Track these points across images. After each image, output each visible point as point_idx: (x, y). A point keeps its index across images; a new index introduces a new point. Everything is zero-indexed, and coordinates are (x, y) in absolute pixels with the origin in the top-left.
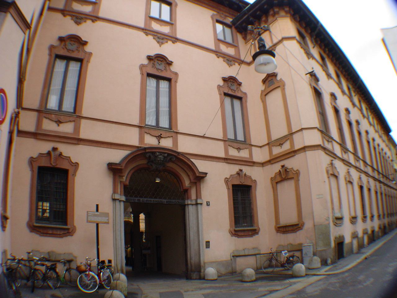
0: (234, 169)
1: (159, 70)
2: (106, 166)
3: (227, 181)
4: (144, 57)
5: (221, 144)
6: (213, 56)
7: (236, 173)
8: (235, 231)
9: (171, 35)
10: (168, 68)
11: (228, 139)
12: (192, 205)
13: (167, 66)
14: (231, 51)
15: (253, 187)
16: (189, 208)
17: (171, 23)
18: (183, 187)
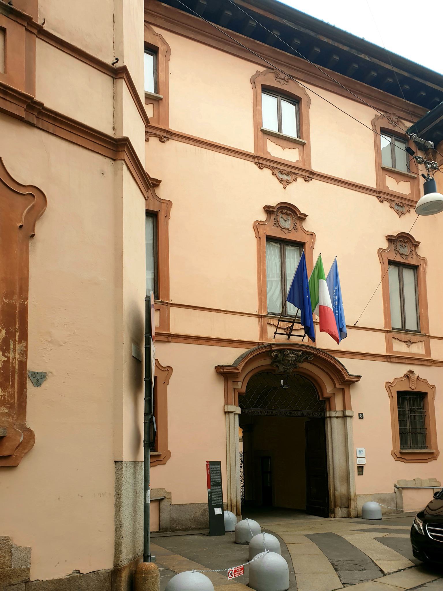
0: (402, 370)
1: (284, 230)
2: (213, 369)
3: (390, 387)
4: (260, 208)
5: (382, 336)
6: (373, 199)
7: (403, 375)
8: (401, 453)
9: (300, 165)
10: (298, 226)
11: (393, 328)
12: (337, 417)
13: (297, 221)
14: (403, 188)
15: (430, 397)
16: (332, 422)
17: (300, 142)
18: (322, 395)
